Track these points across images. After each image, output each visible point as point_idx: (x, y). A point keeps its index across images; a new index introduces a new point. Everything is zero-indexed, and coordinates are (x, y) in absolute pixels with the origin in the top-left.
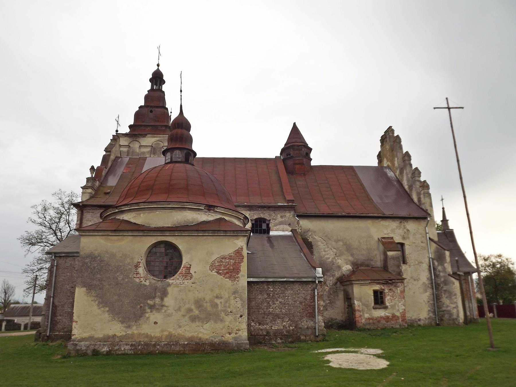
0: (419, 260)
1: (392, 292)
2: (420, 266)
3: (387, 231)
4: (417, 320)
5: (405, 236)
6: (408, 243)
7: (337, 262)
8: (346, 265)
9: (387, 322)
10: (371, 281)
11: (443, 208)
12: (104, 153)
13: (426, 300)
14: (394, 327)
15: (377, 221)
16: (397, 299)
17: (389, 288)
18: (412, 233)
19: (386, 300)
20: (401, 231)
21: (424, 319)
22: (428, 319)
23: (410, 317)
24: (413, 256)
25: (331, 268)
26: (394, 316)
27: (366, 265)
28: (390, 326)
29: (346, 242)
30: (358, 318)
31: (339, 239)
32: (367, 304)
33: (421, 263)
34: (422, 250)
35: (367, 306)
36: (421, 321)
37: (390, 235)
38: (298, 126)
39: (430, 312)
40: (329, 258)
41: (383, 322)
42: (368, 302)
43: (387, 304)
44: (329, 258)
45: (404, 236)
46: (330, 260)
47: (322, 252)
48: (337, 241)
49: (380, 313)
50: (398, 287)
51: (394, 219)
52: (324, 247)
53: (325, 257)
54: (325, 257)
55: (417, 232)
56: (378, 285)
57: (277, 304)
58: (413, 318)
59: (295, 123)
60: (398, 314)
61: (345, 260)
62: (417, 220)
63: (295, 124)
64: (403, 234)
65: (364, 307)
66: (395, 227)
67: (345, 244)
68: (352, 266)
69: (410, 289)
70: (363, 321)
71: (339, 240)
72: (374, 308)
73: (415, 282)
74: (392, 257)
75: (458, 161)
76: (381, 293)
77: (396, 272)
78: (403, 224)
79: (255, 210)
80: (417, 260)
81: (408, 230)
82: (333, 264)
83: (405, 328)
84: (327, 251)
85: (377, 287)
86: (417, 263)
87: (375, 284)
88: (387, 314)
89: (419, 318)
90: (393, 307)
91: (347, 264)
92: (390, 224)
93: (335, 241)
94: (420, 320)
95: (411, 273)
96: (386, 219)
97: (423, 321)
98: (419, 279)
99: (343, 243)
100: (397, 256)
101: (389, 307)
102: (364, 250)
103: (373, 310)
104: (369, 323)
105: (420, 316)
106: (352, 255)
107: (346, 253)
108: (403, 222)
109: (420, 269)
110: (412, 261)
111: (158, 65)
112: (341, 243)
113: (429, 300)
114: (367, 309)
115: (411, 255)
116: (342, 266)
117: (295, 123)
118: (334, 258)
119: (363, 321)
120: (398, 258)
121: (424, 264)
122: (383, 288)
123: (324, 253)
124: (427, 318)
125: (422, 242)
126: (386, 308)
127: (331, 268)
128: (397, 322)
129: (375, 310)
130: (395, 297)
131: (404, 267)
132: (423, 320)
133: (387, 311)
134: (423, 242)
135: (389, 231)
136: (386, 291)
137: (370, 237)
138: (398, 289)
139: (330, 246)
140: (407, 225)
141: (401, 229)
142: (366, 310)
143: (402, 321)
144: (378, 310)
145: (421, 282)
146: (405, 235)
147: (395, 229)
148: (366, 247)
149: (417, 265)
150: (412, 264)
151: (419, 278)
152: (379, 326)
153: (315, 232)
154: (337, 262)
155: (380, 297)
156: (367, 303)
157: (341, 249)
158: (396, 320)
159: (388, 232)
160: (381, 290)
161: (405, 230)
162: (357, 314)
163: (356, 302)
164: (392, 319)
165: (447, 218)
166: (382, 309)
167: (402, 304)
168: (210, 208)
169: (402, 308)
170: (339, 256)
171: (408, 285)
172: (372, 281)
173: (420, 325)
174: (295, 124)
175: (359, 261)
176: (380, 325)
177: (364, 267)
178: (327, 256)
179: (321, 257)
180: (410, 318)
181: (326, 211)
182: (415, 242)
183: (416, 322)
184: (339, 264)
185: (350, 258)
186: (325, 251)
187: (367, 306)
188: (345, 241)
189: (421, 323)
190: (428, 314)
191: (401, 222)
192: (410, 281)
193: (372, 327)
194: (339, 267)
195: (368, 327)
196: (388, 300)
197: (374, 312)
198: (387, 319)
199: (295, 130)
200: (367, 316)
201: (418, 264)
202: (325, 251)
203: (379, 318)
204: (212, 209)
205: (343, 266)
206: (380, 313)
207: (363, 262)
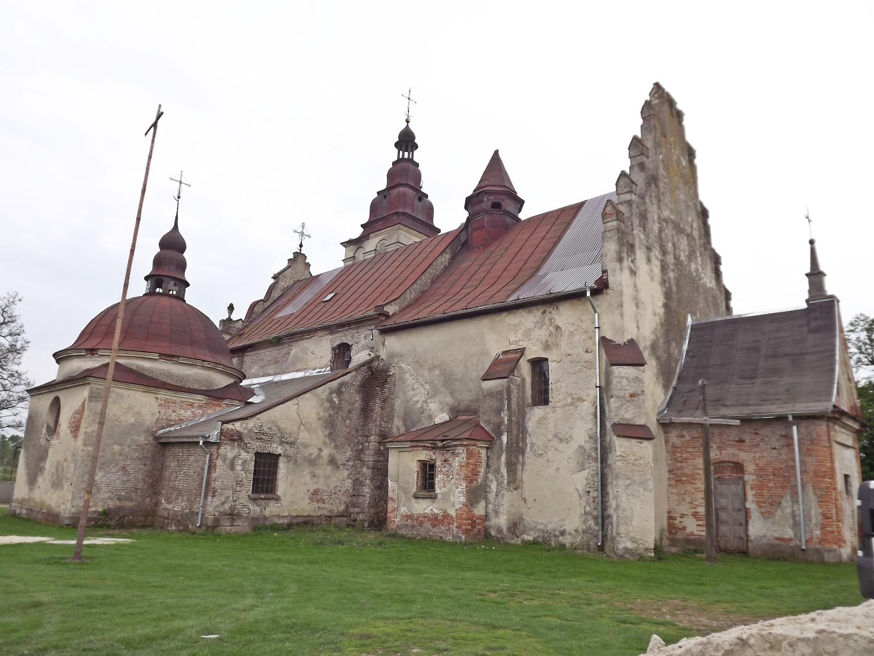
0: (576, 394)
1: (447, 466)
2: (577, 407)
3: (516, 337)
4: (557, 533)
5: (549, 343)
6: (555, 358)
7: (429, 408)
8: (440, 412)
9: (434, 526)
10: (412, 443)
11: (812, 242)
12: (272, 281)
13: (580, 488)
14: (444, 538)
15: (499, 318)
16: (453, 481)
17: (443, 458)
18: (567, 333)
19: (436, 482)
20: (542, 334)
21: (574, 532)
22: (583, 532)
23: (542, 525)
24: (563, 386)
25: (419, 420)
26: (446, 516)
27: (472, 412)
28: (439, 536)
29: (445, 369)
30: (390, 513)
31: (435, 364)
32: (406, 489)
33: (86, 428)
34: (584, 369)
35: (405, 491)
36: (565, 536)
37: (521, 343)
38: (501, 155)
39: (590, 517)
40: (418, 402)
41: (428, 525)
42: (408, 484)
43: (438, 491)
44: (418, 402)
45: (547, 341)
46: (419, 405)
47: (409, 391)
48: (431, 369)
49: (423, 507)
50: (457, 455)
51: (529, 308)
52: (413, 381)
53: (414, 399)
54: (414, 399)
55: (576, 330)
56: (426, 452)
57: (182, 473)
58: (550, 527)
59: (498, 150)
60: (452, 513)
61: (441, 403)
62: (579, 300)
63: (496, 152)
64: (544, 338)
65: (401, 493)
66: (532, 325)
67: (443, 373)
68: (450, 415)
69: (548, 461)
70: (397, 520)
71: (435, 367)
72: (416, 497)
73: (562, 447)
74: (490, 391)
75: (138, 219)
76: (432, 467)
77: (493, 424)
78: (548, 315)
79: (337, 332)
80: (571, 394)
81: (558, 328)
82: (423, 413)
83: (461, 542)
84: (416, 389)
85: (424, 455)
86: (569, 400)
87: (421, 449)
88: (436, 511)
89: (562, 529)
90: (446, 496)
91: (442, 410)
92: (523, 320)
93: (428, 369)
94: (563, 533)
95: (556, 425)
96: (515, 311)
97: (569, 537)
98: (570, 439)
99: (440, 370)
100: (498, 389)
101: (439, 496)
102: (472, 380)
103: (414, 500)
104: (407, 525)
105: (565, 525)
106: (452, 393)
107: (443, 389)
108: (548, 312)
109: (576, 416)
110: (561, 397)
111: (408, 122)
112: (437, 372)
113: (588, 489)
114: (406, 498)
115: (559, 384)
116: (434, 414)
117: (498, 150)
118: (426, 401)
119: (397, 520)
120: (500, 393)
121: (586, 403)
122: (434, 457)
123: (411, 393)
124: (580, 530)
125: (587, 351)
126: (434, 498)
127: (419, 420)
128: (449, 529)
129: (416, 501)
130: (451, 477)
131: (538, 412)
132: (570, 534)
133: (434, 505)
134: (589, 350)
135: (520, 336)
136: (438, 463)
137: (484, 353)
138: (457, 459)
139: (421, 380)
140: (556, 317)
141: (544, 327)
142: (404, 499)
143: (457, 527)
144: (420, 500)
145: (574, 446)
146: (549, 339)
147: (531, 328)
148: (475, 375)
149: (570, 405)
150: (559, 404)
151: (570, 437)
152: (420, 532)
153: (402, 356)
154: (429, 408)
155: (429, 474)
156: (407, 486)
157: (435, 383)
158: (449, 524)
159: (517, 339)
160: (432, 462)
161: (552, 328)
162: (391, 506)
163: (390, 483)
164: (442, 522)
165: (822, 267)
166: (427, 500)
167: (460, 492)
168: (93, 353)
169: (459, 500)
170: (433, 396)
171: (546, 452)
172: (415, 444)
173: (562, 546)
174: (496, 152)
175: (462, 404)
176: (422, 532)
177: (470, 415)
178: (415, 399)
179: (408, 401)
180: (542, 527)
181: (459, 309)
182: (570, 352)
183: (555, 536)
184: (431, 412)
185: (449, 400)
186: (413, 389)
187: (405, 491)
188: (443, 368)
189: (567, 540)
190: (585, 522)
191: (544, 312)
192: (552, 443)
193: (410, 533)
194: (430, 417)
195: (403, 532)
196: (439, 481)
197: (415, 505)
198: (435, 520)
199: (496, 162)
200: (403, 510)
201: (572, 404)
202: (413, 389)
203: (421, 517)
204: (95, 352)
205: (436, 416)
206: (423, 507)
207: (467, 406)
